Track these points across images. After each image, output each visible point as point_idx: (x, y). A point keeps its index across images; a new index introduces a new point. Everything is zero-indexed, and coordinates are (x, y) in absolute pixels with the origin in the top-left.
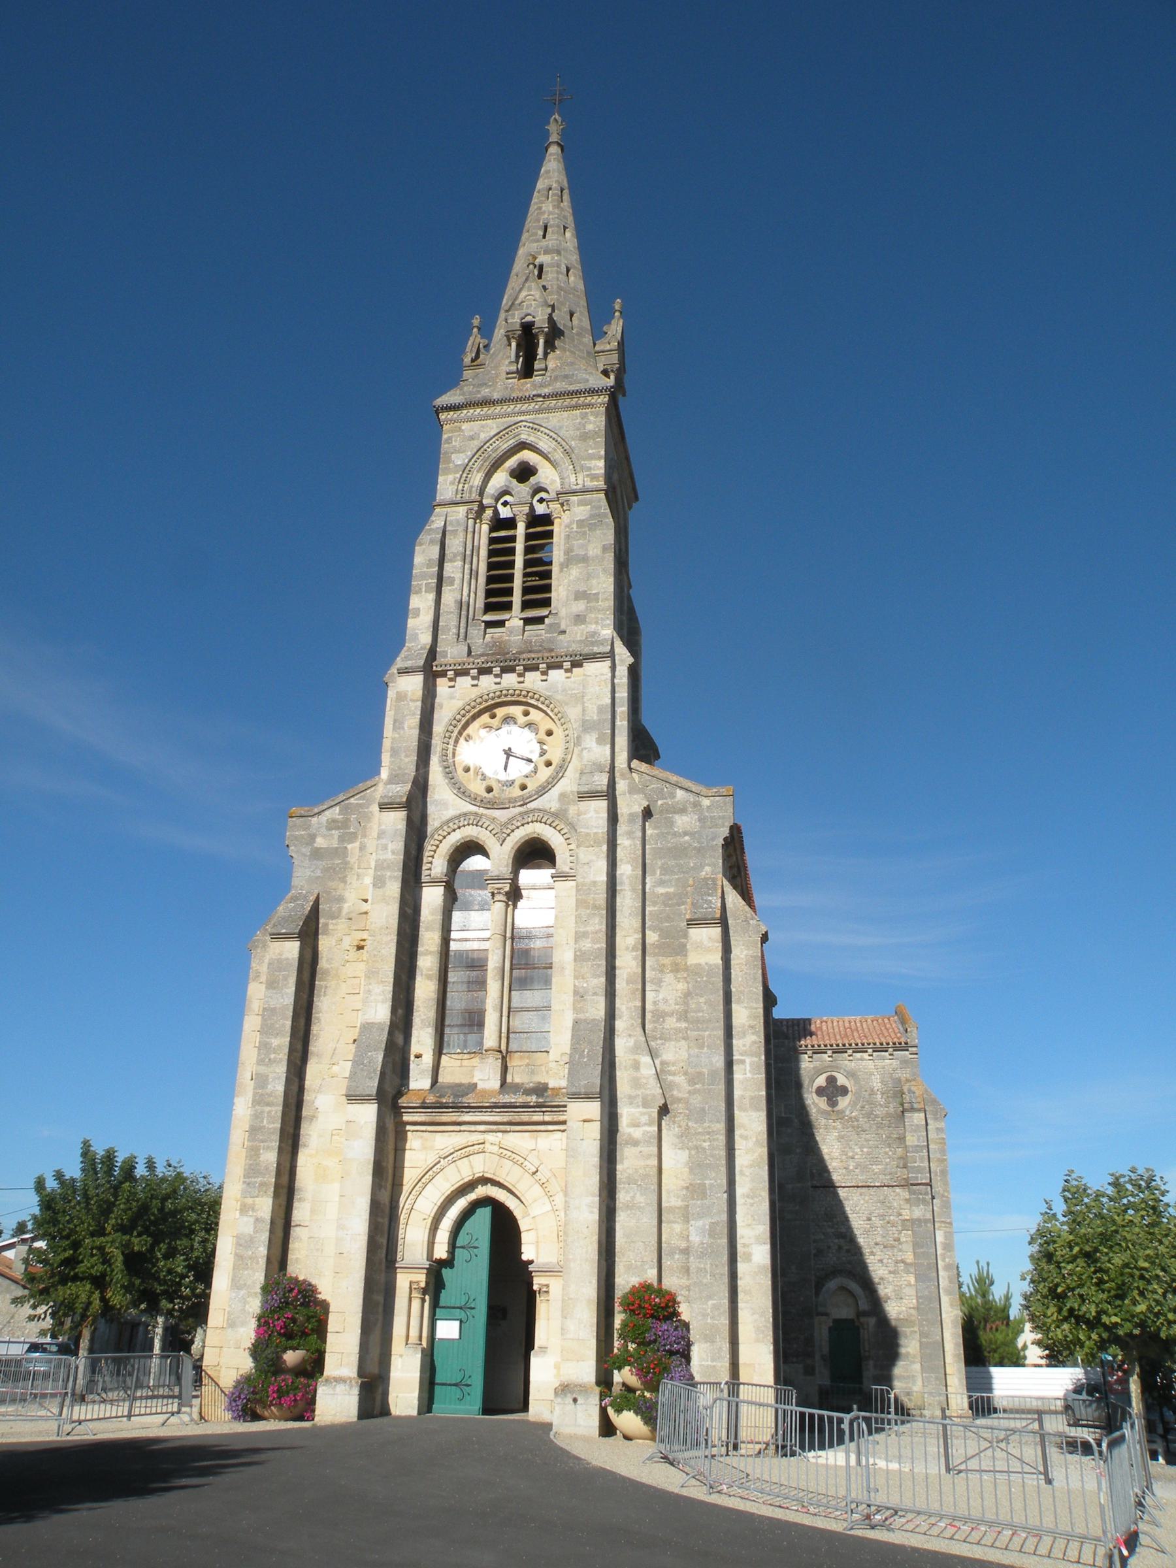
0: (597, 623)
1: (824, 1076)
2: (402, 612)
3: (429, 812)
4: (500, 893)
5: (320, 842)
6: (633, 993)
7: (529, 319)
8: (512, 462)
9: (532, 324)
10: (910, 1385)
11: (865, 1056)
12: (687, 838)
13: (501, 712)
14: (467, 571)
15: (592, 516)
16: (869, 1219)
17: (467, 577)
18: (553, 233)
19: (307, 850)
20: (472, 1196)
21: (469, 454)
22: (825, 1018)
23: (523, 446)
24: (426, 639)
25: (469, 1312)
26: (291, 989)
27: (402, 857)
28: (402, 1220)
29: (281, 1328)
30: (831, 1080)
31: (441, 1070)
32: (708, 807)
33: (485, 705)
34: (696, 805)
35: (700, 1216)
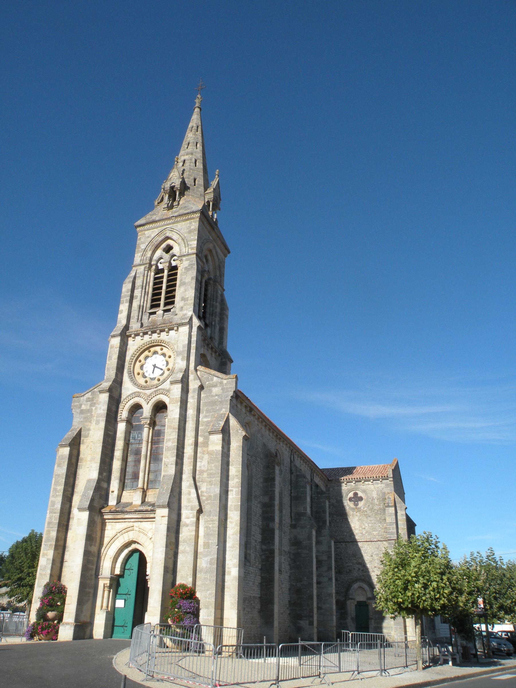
0: (187, 310)
1: (352, 493)
2: (116, 311)
3: (122, 392)
4: (146, 424)
5: (83, 407)
6: (190, 463)
7: (173, 184)
8: (164, 245)
9: (174, 186)
10: (390, 631)
11: (370, 483)
12: (217, 397)
13: (152, 349)
14: (143, 292)
15: (189, 265)
16: (372, 556)
17: (143, 295)
18: (191, 146)
19: (78, 411)
20: (130, 549)
21: (147, 244)
22: (362, 466)
23: (167, 238)
24: (124, 322)
25: (128, 596)
26: (65, 467)
27: (106, 412)
28: (102, 559)
29: (47, 602)
30: (356, 494)
31: (122, 497)
32: (226, 384)
33: (146, 347)
34: (221, 383)
35: (206, 556)
